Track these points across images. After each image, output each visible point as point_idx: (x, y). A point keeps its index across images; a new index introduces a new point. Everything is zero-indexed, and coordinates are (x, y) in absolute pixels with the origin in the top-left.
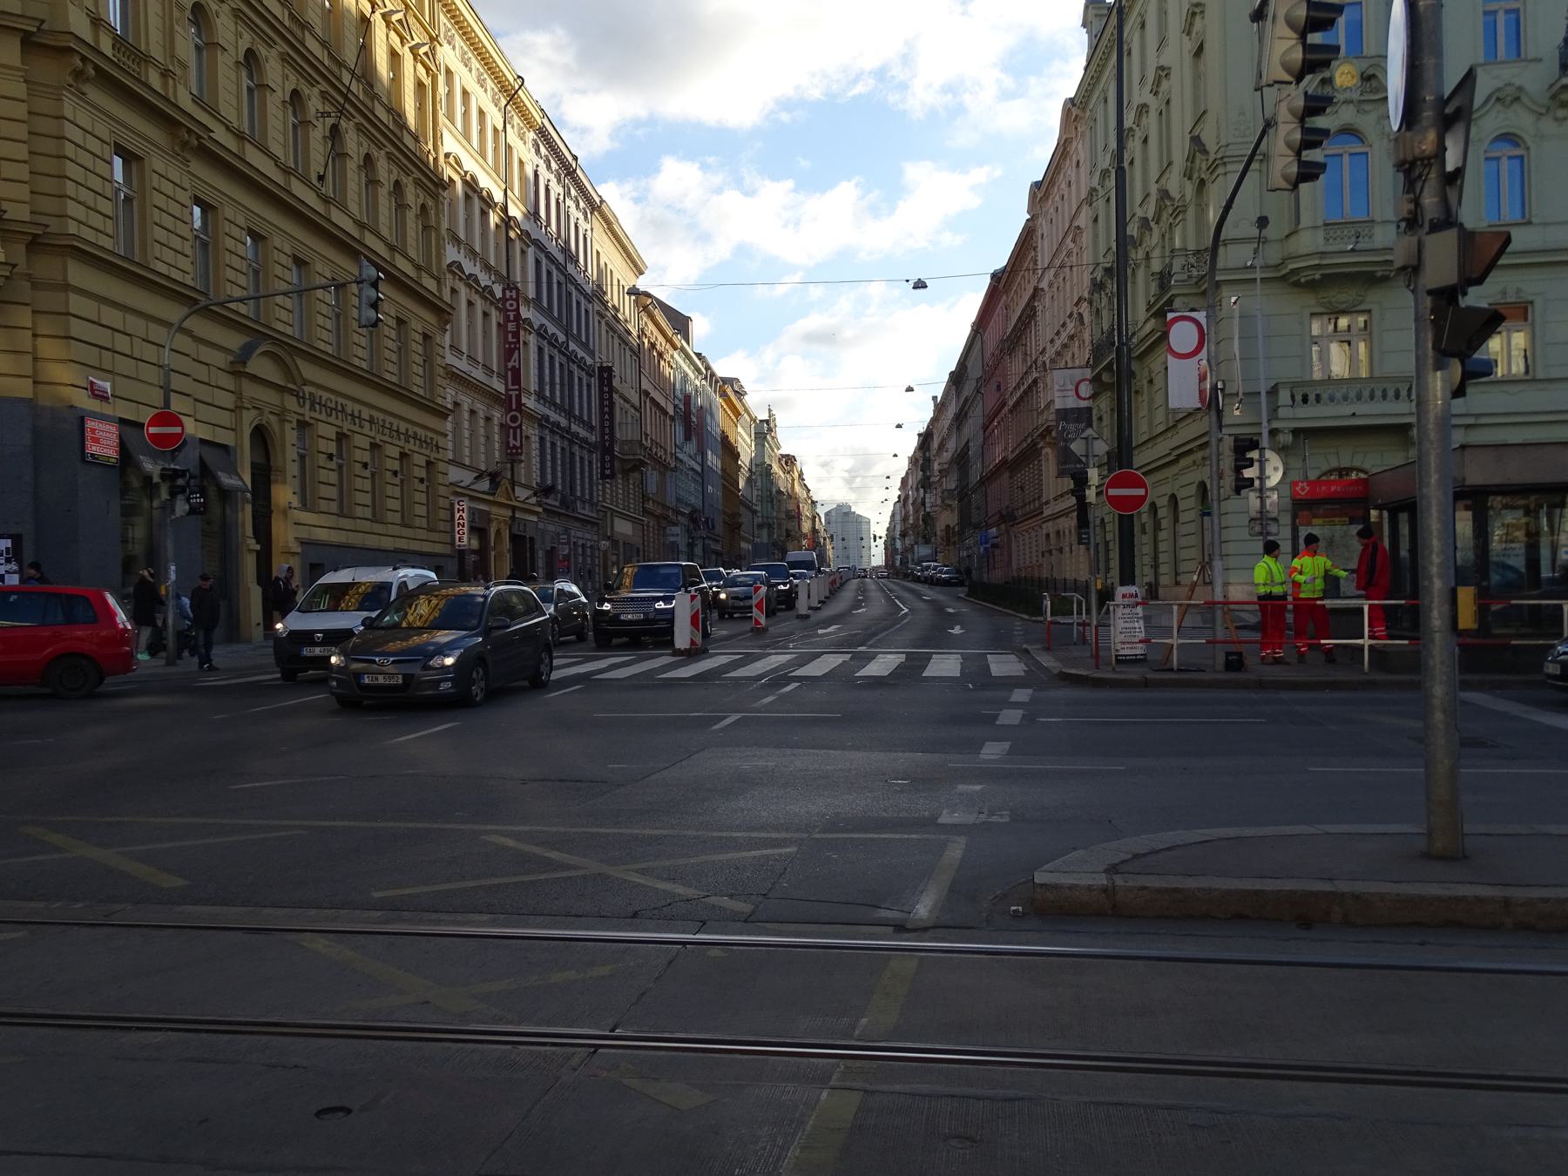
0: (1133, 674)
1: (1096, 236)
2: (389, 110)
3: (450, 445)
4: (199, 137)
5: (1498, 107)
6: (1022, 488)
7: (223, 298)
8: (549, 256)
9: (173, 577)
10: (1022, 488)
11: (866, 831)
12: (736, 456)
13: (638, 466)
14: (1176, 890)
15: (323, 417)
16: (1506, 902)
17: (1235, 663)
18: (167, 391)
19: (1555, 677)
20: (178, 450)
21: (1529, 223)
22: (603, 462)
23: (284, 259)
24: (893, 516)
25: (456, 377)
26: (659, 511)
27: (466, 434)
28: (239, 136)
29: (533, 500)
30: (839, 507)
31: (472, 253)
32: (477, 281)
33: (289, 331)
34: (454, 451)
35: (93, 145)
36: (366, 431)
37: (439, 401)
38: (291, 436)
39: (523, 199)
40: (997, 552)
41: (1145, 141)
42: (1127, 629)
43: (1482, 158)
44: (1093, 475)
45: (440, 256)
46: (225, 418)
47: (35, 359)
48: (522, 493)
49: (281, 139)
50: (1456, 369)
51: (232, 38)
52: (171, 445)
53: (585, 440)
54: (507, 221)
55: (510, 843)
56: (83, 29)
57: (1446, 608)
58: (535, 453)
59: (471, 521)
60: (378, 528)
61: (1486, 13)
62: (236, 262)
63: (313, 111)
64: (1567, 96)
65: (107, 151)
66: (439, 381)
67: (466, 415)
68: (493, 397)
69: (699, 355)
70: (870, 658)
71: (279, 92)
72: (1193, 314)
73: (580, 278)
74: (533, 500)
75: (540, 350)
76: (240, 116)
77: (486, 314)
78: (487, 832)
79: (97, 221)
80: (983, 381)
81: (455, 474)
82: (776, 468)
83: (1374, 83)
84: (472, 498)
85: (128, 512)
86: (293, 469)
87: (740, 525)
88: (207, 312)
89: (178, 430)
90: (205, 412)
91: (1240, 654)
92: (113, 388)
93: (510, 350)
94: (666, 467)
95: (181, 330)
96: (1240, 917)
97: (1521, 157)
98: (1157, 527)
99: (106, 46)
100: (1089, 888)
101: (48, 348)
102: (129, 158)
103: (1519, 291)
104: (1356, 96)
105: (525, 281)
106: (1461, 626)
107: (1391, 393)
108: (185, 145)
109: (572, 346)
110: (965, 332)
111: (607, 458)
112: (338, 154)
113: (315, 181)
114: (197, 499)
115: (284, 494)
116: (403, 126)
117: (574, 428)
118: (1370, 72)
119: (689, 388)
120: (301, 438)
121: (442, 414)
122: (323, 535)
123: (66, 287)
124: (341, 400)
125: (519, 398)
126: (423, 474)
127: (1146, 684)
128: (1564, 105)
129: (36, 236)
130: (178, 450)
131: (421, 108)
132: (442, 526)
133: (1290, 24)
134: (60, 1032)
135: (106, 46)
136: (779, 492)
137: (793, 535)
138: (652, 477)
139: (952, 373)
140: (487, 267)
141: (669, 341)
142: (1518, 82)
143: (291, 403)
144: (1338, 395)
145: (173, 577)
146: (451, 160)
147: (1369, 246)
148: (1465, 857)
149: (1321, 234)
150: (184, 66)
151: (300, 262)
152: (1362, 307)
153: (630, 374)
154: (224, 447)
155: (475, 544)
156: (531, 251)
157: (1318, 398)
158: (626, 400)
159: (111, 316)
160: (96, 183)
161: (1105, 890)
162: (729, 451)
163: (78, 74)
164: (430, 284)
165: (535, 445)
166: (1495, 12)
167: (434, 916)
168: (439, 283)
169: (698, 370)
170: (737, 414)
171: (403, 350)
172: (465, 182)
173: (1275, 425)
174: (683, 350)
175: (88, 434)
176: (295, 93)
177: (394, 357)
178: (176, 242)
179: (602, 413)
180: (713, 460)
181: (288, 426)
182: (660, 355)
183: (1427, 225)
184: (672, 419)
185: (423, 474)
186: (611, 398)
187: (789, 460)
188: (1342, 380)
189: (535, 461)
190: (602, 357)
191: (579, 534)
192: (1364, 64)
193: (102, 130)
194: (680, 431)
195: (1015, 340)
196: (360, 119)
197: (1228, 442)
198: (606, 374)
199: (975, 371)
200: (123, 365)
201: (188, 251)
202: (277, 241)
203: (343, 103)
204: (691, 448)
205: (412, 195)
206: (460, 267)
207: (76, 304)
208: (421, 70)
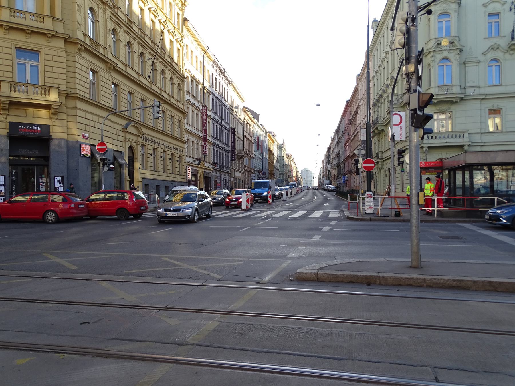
0: (367, 217)
1: (374, 90)
2: (169, 57)
3: (186, 151)
4: (114, 66)
5: (492, 51)
7: (120, 110)
8: (216, 98)
9: (104, 188)
11: (265, 258)
12: (273, 154)
13: (242, 157)
14: (334, 275)
15: (149, 143)
16: (425, 279)
17: (398, 214)
18: (102, 136)
19: (487, 219)
20: (105, 153)
21: (501, 85)
22: (232, 156)
23: (138, 100)
25: (188, 132)
26: (249, 170)
27: (191, 148)
28: (126, 65)
29: (211, 167)
31: (193, 97)
32: (194, 105)
33: (139, 119)
34: (188, 153)
35: (84, 69)
36: (162, 147)
37: (183, 139)
38: (140, 148)
39: (209, 81)
41: (388, 62)
42: (368, 204)
43: (487, 65)
44: (360, 160)
45: (183, 98)
46: (121, 144)
47: (67, 128)
48: (207, 165)
49: (137, 66)
50: (421, 131)
51: (124, 38)
52: (103, 151)
53: (227, 150)
54: (204, 88)
55: (168, 260)
56: (81, 37)
57: (416, 198)
58: (212, 153)
59: (192, 172)
60: (165, 174)
61: (489, 23)
62: (124, 100)
63: (147, 58)
64: (513, 47)
65: (88, 70)
66: (183, 133)
67: (191, 143)
68: (199, 138)
69: (262, 125)
70: (297, 212)
71: (137, 53)
72: (399, 113)
73: (226, 104)
74: (211, 167)
75: (213, 124)
76: (126, 60)
77: (197, 114)
78: (163, 257)
79: (85, 90)
80: (344, 132)
81: (188, 159)
82: (285, 157)
83: (453, 44)
84: (192, 166)
85: (93, 170)
86: (140, 158)
87: (273, 174)
88: (115, 114)
89: (105, 147)
90: (115, 142)
91: (399, 212)
92: (89, 135)
93: (204, 124)
94: (251, 157)
95: (106, 119)
96: (352, 282)
97: (499, 66)
98: (390, 175)
99: (88, 42)
100: (311, 273)
101: (71, 125)
102: (94, 72)
103: (498, 105)
104: (448, 48)
105: (209, 105)
106: (420, 203)
107: (458, 136)
108: (110, 68)
109: (223, 123)
112: (154, 70)
113: (147, 77)
114: (112, 166)
115: (138, 165)
116: (173, 61)
117: (223, 146)
118: (453, 41)
119: (258, 135)
120: (143, 149)
121: (184, 143)
122: (149, 176)
123: (76, 108)
124: (154, 139)
125: (206, 137)
126: (178, 159)
127: (371, 220)
128: (512, 50)
129: (68, 94)
130: (105, 153)
131: (178, 56)
132: (184, 174)
133: (401, 32)
134: (29, 303)
135: (88, 42)
136: (286, 164)
137: (290, 177)
138: (247, 160)
140: (198, 101)
141: (252, 121)
142: (498, 43)
143: (140, 139)
144: (442, 137)
145: (104, 188)
146: (187, 71)
147: (452, 92)
148: (421, 268)
149: (437, 89)
150: (110, 46)
151: (143, 100)
152: (450, 110)
153: (241, 131)
154: (121, 152)
155: (193, 179)
156: (211, 96)
157: (436, 137)
158: (239, 138)
159: (89, 116)
160: (84, 79)
161: (315, 274)
162: (271, 152)
163: (80, 50)
164: (181, 106)
165: (212, 151)
166: (492, 23)
167: (137, 277)
168: (183, 105)
169: (261, 129)
170: (273, 142)
171: (172, 124)
172: (191, 77)
173: (422, 145)
174: (256, 123)
175: (82, 149)
176: (142, 53)
177: (170, 127)
178: (107, 95)
179: (232, 142)
180: (266, 155)
181: (139, 146)
182: (250, 125)
183: (412, 91)
184: (253, 143)
185: (178, 159)
186: (234, 138)
187: (289, 156)
188: (443, 132)
189: (212, 155)
190: (232, 126)
191: (224, 176)
192: (451, 39)
193: (86, 65)
194: (255, 147)
195: (353, 120)
196: (160, 60)
197: (396, 151)
198: (233, 131)
199: (342, 129)
200: (92, 129)
201: (111, 98)
202: (136, 95)
203: (155, 55)
204: (259, 152)
205: (176, 81)
206: (190, 101)
207: (79, 113)
208: (179, 46)
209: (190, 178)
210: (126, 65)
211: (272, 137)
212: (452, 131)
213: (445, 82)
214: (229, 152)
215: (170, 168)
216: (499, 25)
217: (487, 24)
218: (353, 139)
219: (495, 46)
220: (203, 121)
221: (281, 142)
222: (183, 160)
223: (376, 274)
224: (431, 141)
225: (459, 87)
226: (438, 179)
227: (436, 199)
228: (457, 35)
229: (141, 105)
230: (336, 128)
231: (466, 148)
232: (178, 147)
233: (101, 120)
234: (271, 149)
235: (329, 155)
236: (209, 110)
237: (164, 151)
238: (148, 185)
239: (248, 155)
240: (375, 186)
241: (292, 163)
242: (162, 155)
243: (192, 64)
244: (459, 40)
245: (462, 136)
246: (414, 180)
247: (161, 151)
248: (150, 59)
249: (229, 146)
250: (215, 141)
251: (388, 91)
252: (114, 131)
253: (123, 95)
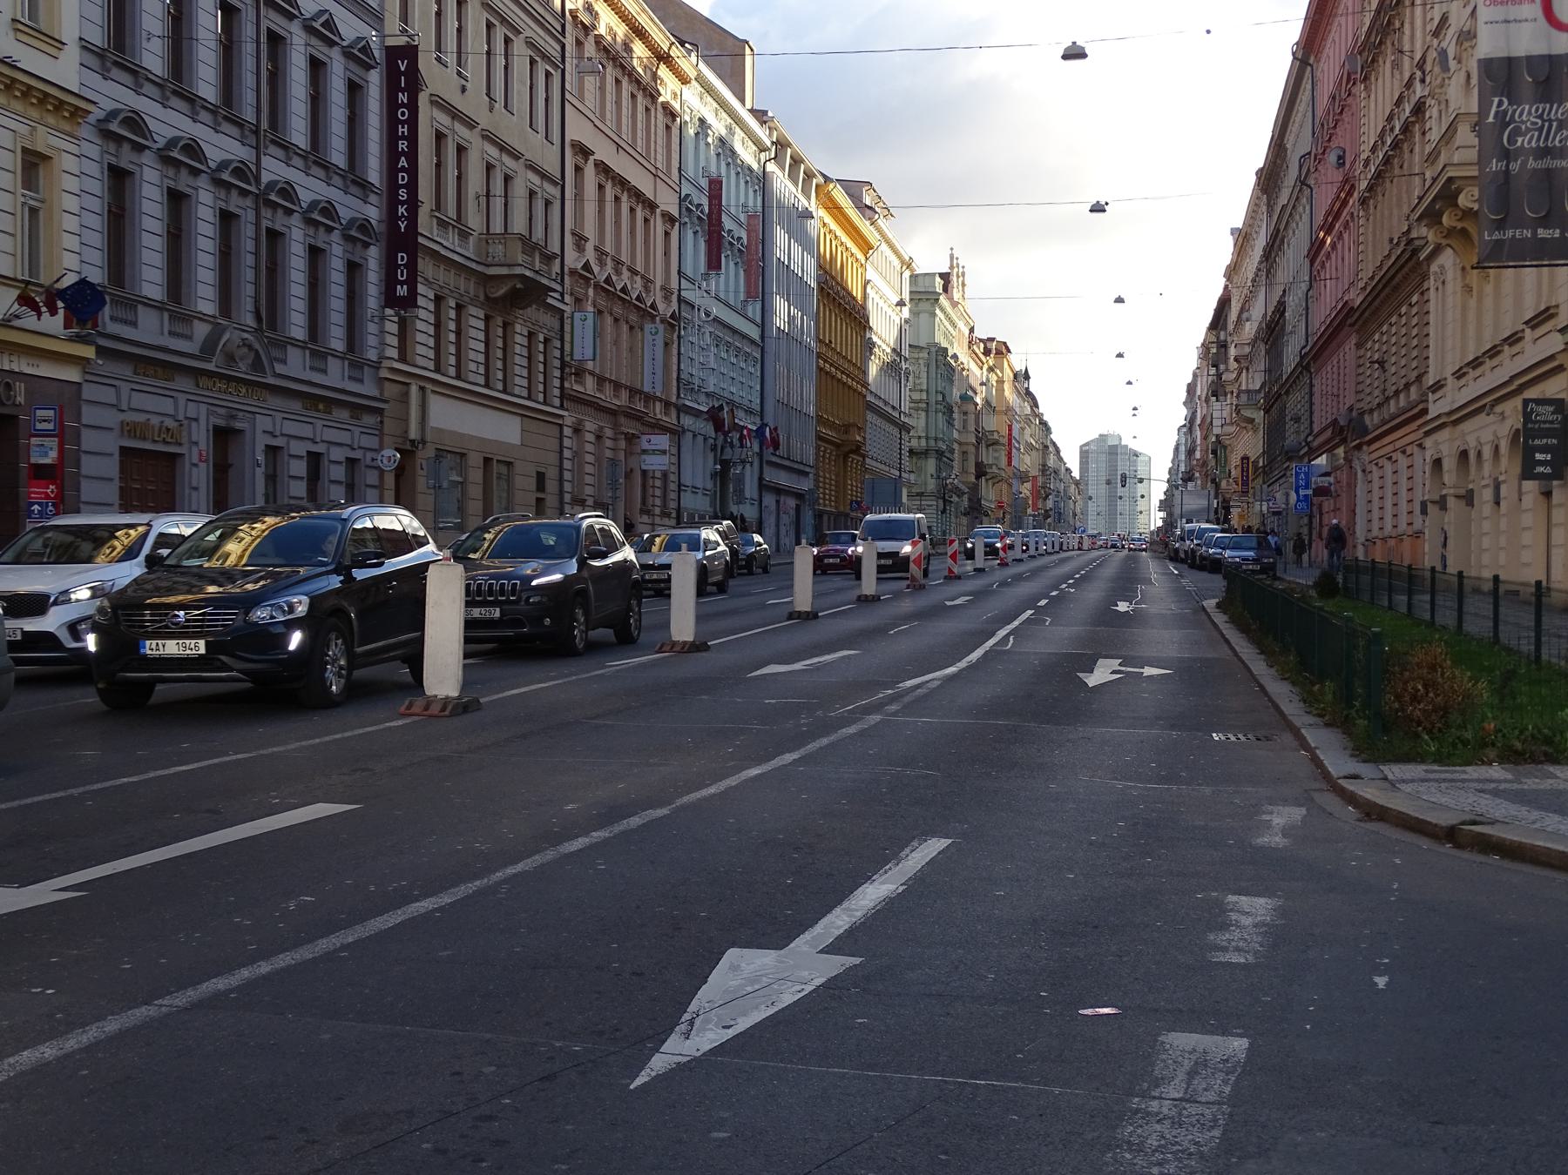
6: (1381, 363)
10: (1381, 363)
24: (1177, 449)
30: (1103, 438)
40: (1328, 504)
69: (760, 115)
94: (648, 314)
110: (1282, 64)
111: (402, 258)
139: (1260, 173)
170: (866, 247)
187: (996, 350)
194: (694, 251)
230: (1258, 156)
235: (1223, 346)
249: (364, 186)
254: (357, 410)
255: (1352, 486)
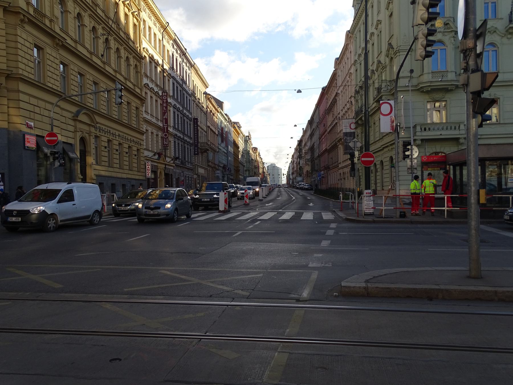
0: (370, 219)
1: (357, 75)
2: (125, 33)
3: (145, 144)
4: (62, 42)
7: (70, 95)
8: (177, 82)
12: (238, 148)
13: (206, 151)
15: (103, 134)
16: (496, 292)
17: (403, 215)
19: (508, 220)
20: (56, 145)
22: (195, 149)
23: (90, 82)
24: (289, 167)
26: (213, 166)
27: (150, 140)
28: (75, 42)
30: (272, 164)
31: (152, 81)
32: (153, 90)
33: (92, 106)
34: (146, 146)
35: (27, 44)
36: (117, 139)
37: (141, 129)
38: (93, 140)
40: (323, 179)
41: (373, 44)
42: (367, 204)
44: (357, 154)
45: (141, 81)
46: (71, 135)
47: (8, 115)
48: (168, 160)
50: (480, 118)
52: (53, 143)
53: (189, 142)
54: (163, 70)
55: (169, 273)
56: (24, 7)
57: (476, 196)
58: (172, 146)
59: (152, 169)
60: (121, 171)
61: (485, 3)
62: (75, 83)
63: (100, 33)
64: (511, 31)
65: (32, 46)
66: (141, 122)
67: (150, 134)
71: (89, 27)
73: (187, 89)
75: (174, 112)
76: (76, 35)
79: (28, 69)
80: (319, 123)
81: (146, 153)
82: (251, 152)
83: (448, 26)
84: (152, 161)
85: (39, 165)
86: (93, 151)
88: (65, 100)
89: (56, 138)
90: (64, 133)
92: (34, 124)
93: (164, 112)
94: (215, 151)
96: (409, 297)
97: (496, 51)
99: (31, 11)
100: (360, 287)
101: (12, 111)
102: (39, 49)
104: (442, 30)
105: (169, 90)
106: (481, 202)
107: (453, 128)
109: (185, 111)
110: (313, 107)
111: (196, 148)
113: (100, 57)
115: (90, 160)
116: (129, 38)
117: (185, 138)
118: (447, 22)
119: (223, 125)
120: (96, 141)
121: (142, 133)
122: (103, 173)
123: (19, 91)
124: (109, 129)
125: (167, 128)
127: (374, 222)
128: (510, 33)
129: (8, 74)
131: (135, 33)
132: (142, 170)
135: (31, 11)
136: (252, 159)
138: (211, 155)
139: (309, 121)
140: (157, 85)
141: (216, 110)
143: (93, 130)
144: (436, 128)
146: (145, 50)
148: (482, 278)
149: (431, 75)
150: (57, 18)
151: (95, 83)
154: (71, 144)
155: (153, 176)
156: (171, 80)
158: (203, 129)
159: (33, 101)
160: (28, 57)
161: (365, 288)
163: (22, 21)
164: (138, 90)
165: (172, 144)
166: (488, 3)
168: (141, 90)
170: (239, 134)
171: (129, 112)
172: (150, 57)
174: (221, 113)
175: (26, 140)
176: (94, 28)
177: (126, 115)
178: (55, 77)
179: (194, 134)
180: (231, 149)
181: (92, 137)
182: (213, 114)
184: (217, 135)
186: (197, 128)
187: (255, 149)
189: (173, 149)
191: (187, 173)
192: (445, 20)
193: (30, 39)
194: (220, 139)
195: (330, 110)
196: (115, 36)
198: (196, 120)
199: (316, 120)
200: (37, 117)
201: (59, 80)
203: (109, 31)
204: (223, 145)
205: (132, 61)
206: (148, 85)
207: (22, 97)
208: (135, 20)
209: (149, 174)
210: (75, 42)
211: (237, 128)
212: (447, 122)
213: (439, 67)
214: (191, 145)
215: (127, 163)
216: (495, 6)
217: (483, 5)
218: (330, 130)
219: (492, 29)
220: (163, 109)
221: (247, 134)
222: (142, 155)
223: (437, 287)
224: (424, 133)
225: (454, 74)
226: (445, 175)
227: (446, 198)
228: (452, 16)
229: (94, 89)
231: (461, 141)
232: (135, 139)
233: (49, 107)
234: (237, 142)
236: (170, 96)
237: (120, 144)
238: (103, 183)
239: (212, 149)
240: (358, 183)
241: (258, 158)
242: (117, 148)
243: (150, 42)
244: (454, 21)
245: (457, 127)
246: (473, 175)
247: (117, 143)
248: (104, 35)
250: (176, 133)
251: (373, 76)
252: (63, 119)
253: (72, 77)
254: (192, 170)
255: (328, 176)
